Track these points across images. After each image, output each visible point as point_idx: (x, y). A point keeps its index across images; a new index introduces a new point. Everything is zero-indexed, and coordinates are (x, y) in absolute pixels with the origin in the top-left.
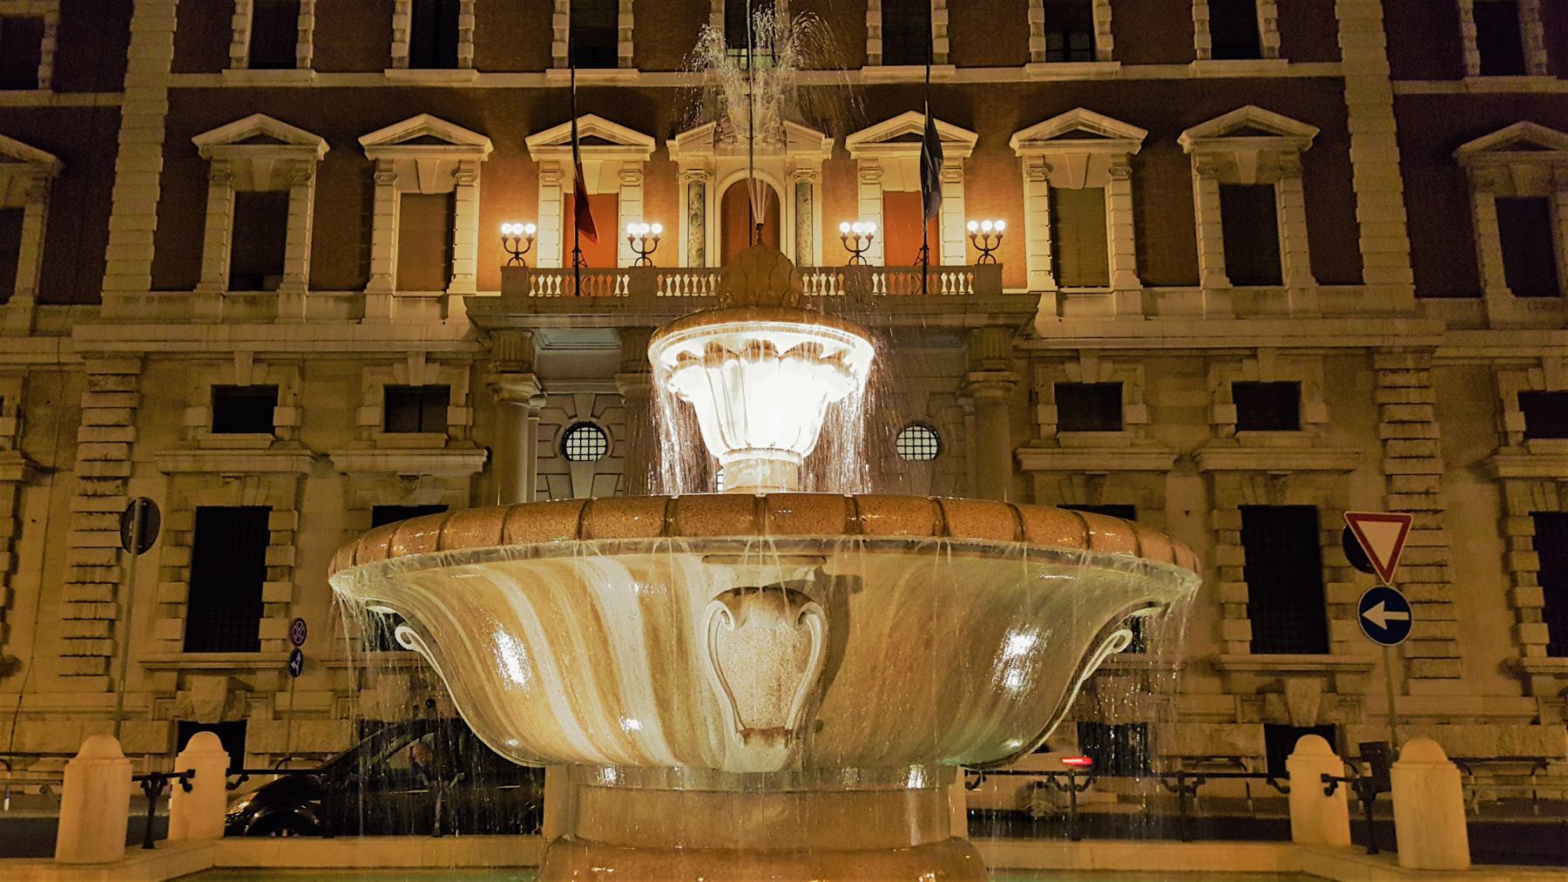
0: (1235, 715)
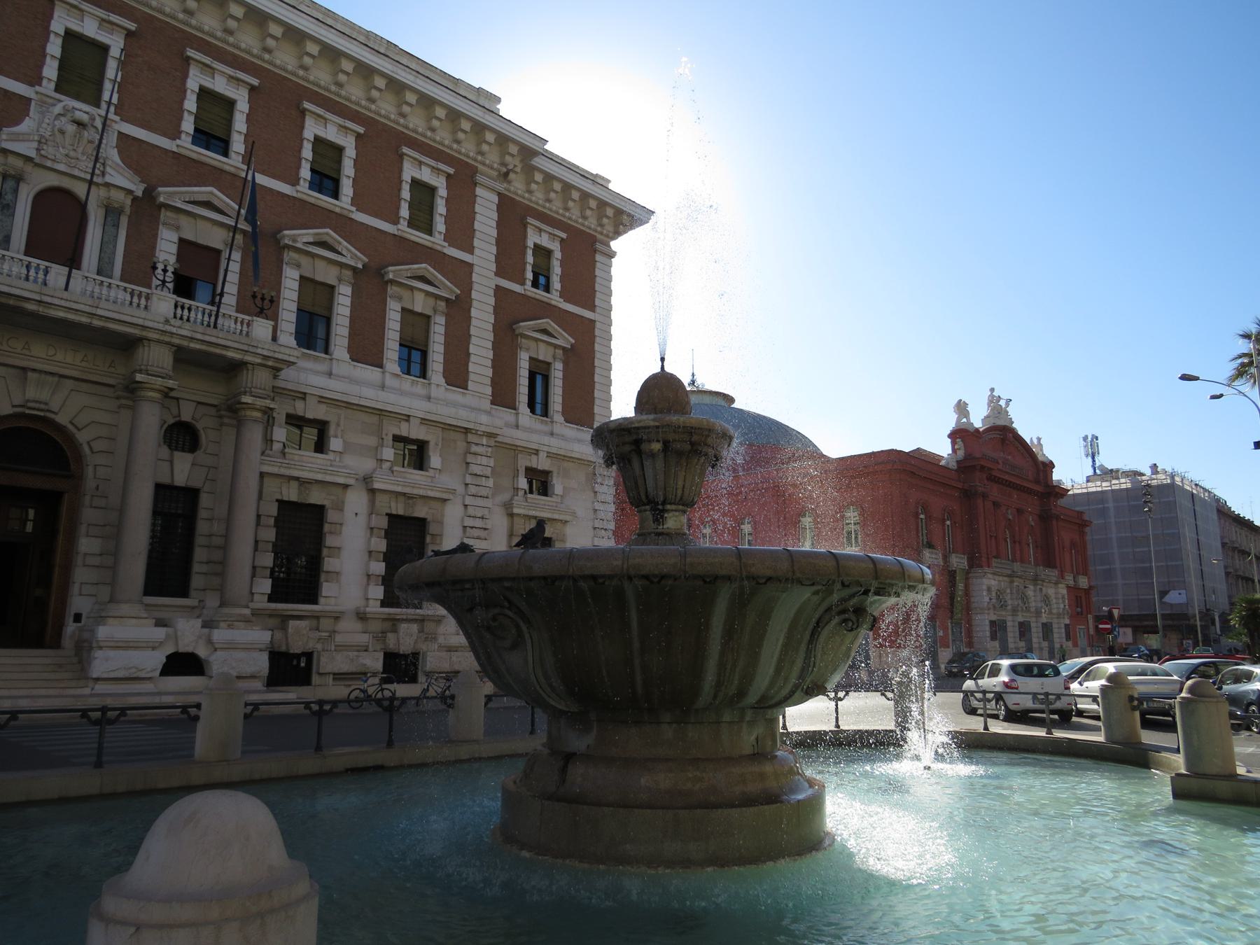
0: (368, 646)
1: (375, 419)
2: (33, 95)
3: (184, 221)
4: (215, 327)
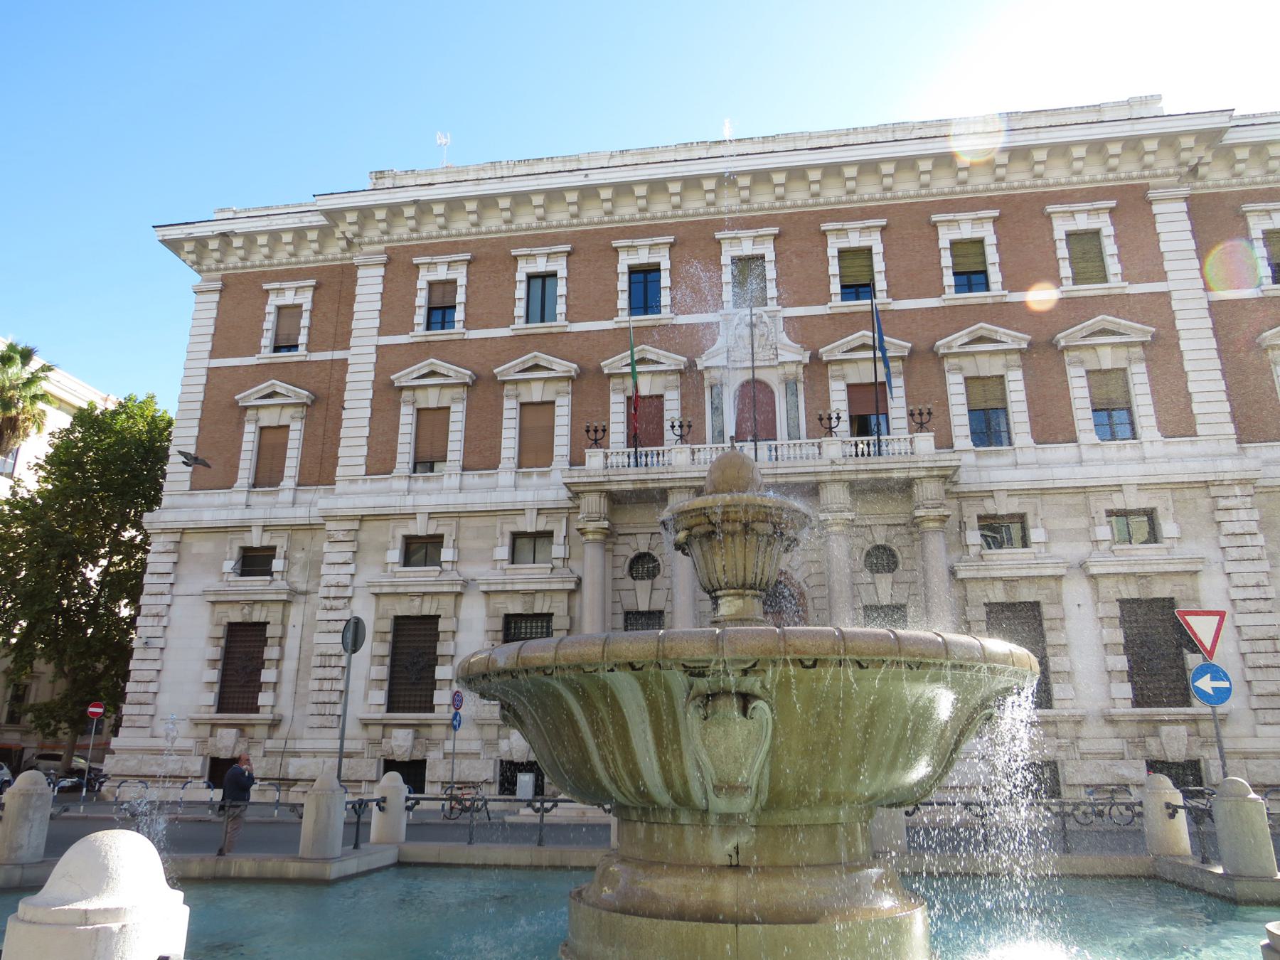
0: (1123, 754)
1: (1080, 498)
2: (720, 319)
3: (848, 368)
4: (880, 454)
